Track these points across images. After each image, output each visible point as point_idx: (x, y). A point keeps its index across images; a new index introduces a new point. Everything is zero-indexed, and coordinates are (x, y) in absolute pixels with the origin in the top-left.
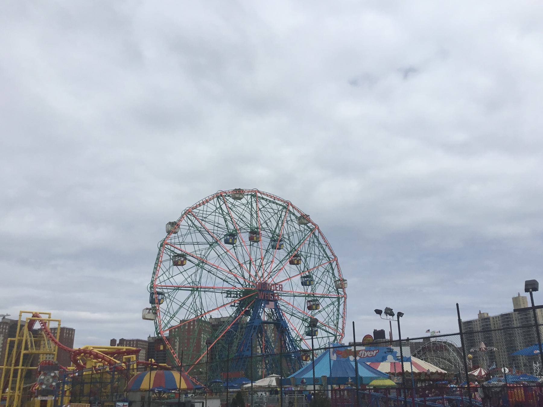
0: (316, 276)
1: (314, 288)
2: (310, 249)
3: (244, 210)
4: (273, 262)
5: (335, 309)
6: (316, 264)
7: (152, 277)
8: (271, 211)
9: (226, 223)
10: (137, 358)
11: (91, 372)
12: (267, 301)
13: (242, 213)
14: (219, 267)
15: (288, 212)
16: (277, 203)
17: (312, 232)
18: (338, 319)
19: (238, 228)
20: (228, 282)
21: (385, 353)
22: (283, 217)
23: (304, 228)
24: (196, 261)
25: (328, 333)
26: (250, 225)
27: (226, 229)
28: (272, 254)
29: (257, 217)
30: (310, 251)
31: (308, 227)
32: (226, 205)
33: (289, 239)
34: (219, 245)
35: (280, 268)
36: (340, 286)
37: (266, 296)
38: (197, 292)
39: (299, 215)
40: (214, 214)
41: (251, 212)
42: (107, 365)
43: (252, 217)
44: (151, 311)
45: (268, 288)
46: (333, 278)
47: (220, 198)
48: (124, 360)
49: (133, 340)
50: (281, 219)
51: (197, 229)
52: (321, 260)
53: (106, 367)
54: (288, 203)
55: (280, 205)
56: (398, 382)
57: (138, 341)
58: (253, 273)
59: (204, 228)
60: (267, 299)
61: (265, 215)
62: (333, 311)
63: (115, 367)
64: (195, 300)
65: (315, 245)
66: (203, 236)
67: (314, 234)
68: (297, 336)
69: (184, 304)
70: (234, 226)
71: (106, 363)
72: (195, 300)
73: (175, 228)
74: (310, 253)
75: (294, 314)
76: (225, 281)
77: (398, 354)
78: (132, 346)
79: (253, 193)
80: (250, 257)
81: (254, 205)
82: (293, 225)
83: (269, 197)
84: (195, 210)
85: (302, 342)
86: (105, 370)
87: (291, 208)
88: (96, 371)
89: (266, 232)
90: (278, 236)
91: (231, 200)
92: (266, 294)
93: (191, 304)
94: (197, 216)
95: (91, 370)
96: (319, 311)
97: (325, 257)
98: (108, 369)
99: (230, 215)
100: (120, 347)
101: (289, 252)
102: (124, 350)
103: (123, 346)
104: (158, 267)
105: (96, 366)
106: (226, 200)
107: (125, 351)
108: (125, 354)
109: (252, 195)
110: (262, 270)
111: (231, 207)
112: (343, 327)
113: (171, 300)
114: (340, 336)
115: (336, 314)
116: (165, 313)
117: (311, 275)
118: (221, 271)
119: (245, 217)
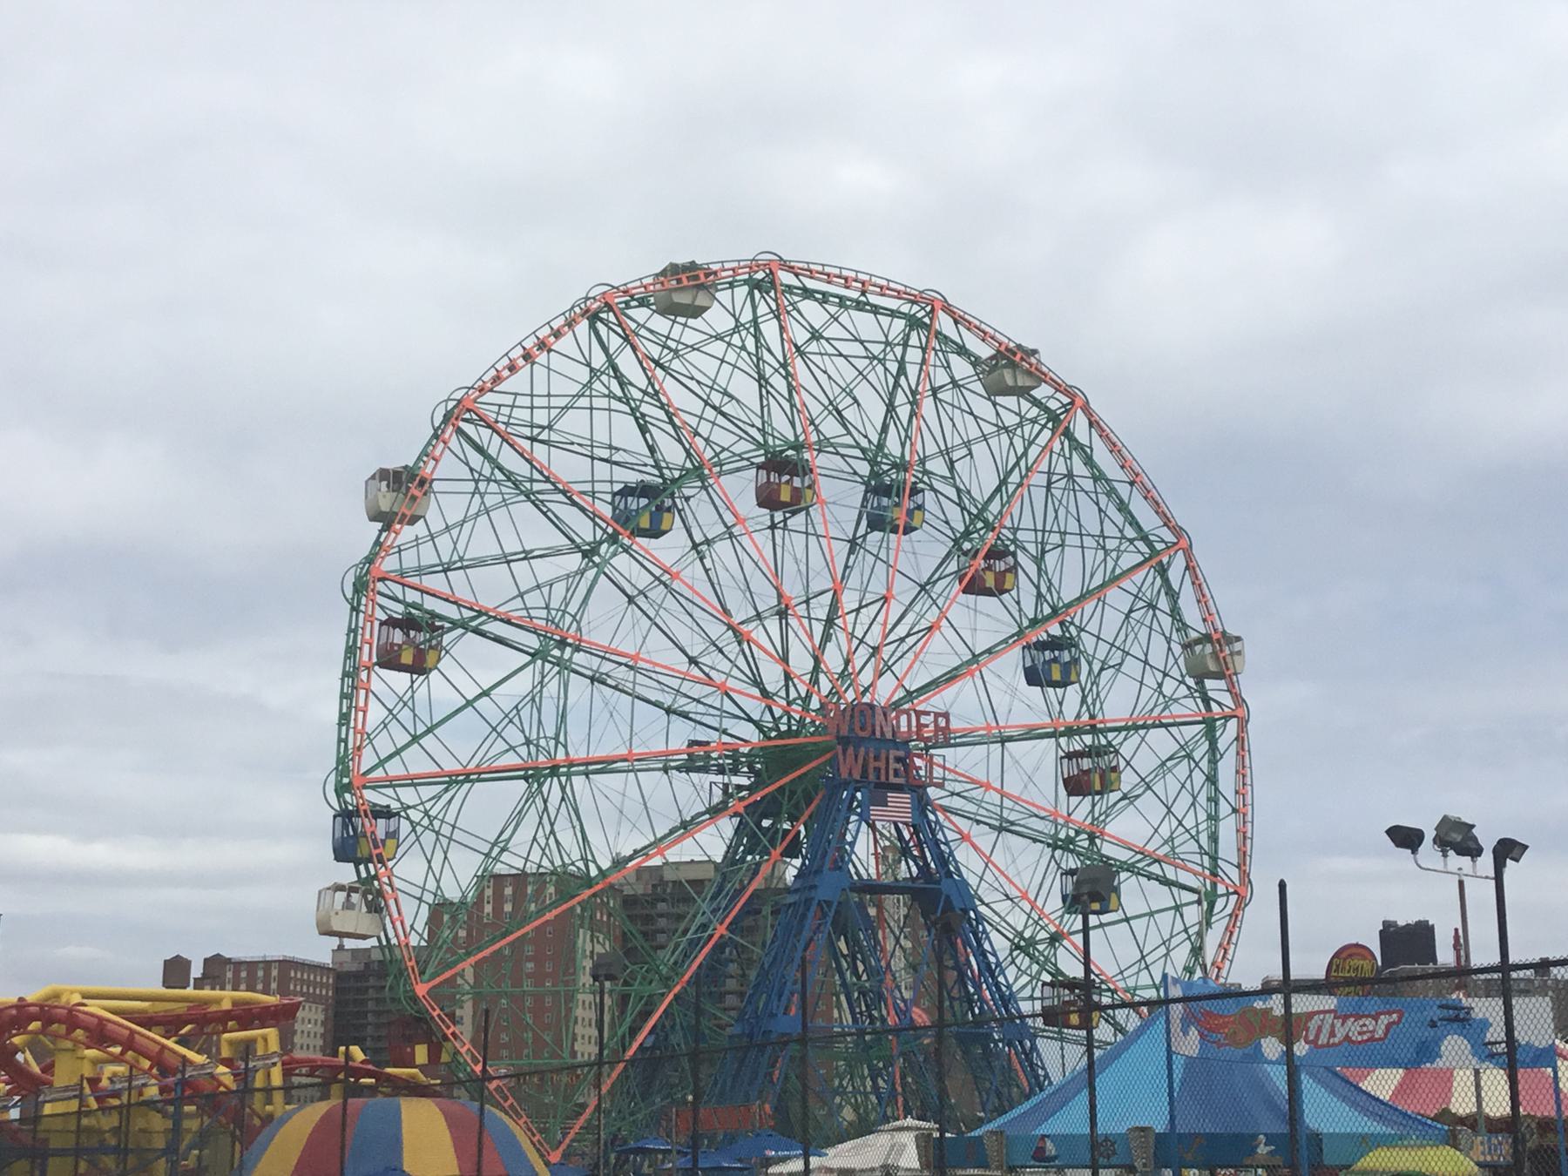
0: (1098, 638)
1: (1094, 688)
2: (1056, 512)
3: (722, 361)
4: (893, 600)
5: (1199, 778)
6: (1092, 576)
7: (340, 740)
8: (854, 349)
9: (648, 435)
10: (286, 1041)
11: (73, 1106)
12: (880, 790)
13: (714, 382)
14: (643, 660)
15: (935, 343)
16: (876, 306)
17: (1061, 429)
18: (1213, 818)
19: (708, 454)
20: (690, 715)
21: (1433, 1025)
22: (912, 371)
23: (1018, 414)
24: (533, 642)
25: (1175, 890)
26: (762, 431)
27: (649, 469)
28: (883, 555)
29: (790, 388)
30: (1056, 517)
31: (1036, 402)
32: (634, 349)
33: (951, 478)
34: (626, 551)
35: (924, 624)
36: (1212, 667)
37: (872, 764)
38: (555, 779)
39: (984, 351)
40: (584, 402)
41: (757, 366)
42: (148, 1072)
43: (768, 392)
44: (355, 897)
45: (882, 728)
46: (1177, 630)
47: (601, 320)
48: (226, 1053)
49: (267, 964)
50: (902, 380)
51: (517, 487)
52: (1114, 554)
53: (143, 1082)
54: (934, 304)
55: (894, 314)
56: (1489, 1158)
57: (287, 965)
58: (801, 662)
59: (547, 480)
60: (879, 778)
61: (825, 372)
62: (1188, 785)
63: (184, 1083)
64: (552, 825)
65: (1077, 488)
66: (544, 514)
67: (1067, 434)
68: (1031, 921)
69: (503, 850)
70: (687, 446)
71: (146, 1064)
72: (552, 825)
73: (414, 498)
74: (1060, 532)
75: (1012, 823)
76: (675, 712)
77: (1491, 1030)
78: (260, 987)
79: (760, 275)
80: (776, 588)
81: (770, 329)
82: (965, 407)
83: (838, 285)
84: (489, 397)
85: (1061, 951)
86: (141, 1094)
87: (945, 324)
88: (97, 1099)
89: (843, 456)
90: (901, 466)
91: (661, 324)
92: (872, 755)
93: (535, 839)
94: (507, 424)
95: (75, 1097)
96: (1125, 797)
97: (1131, 541)
98: (152, 1092)
99: (664, 400)
100: (206, 993)
101: (958, 535)
102: (226, 1005)
103: (223, 988)
104: (363, 693)
105: (99, 1080)
106: (633, 326)
107: (228, 1012)
108: (230, 1023)
109: (754, 285)
110: (842, 637)
111: (660, 359)
112: (1243, 854)
113: (438, 833)
114: (1233, 898)
115: (1202, 799)
116: (420, 899)
117: (1071, 638)
118: (653, 675)
119: (732, 397)
